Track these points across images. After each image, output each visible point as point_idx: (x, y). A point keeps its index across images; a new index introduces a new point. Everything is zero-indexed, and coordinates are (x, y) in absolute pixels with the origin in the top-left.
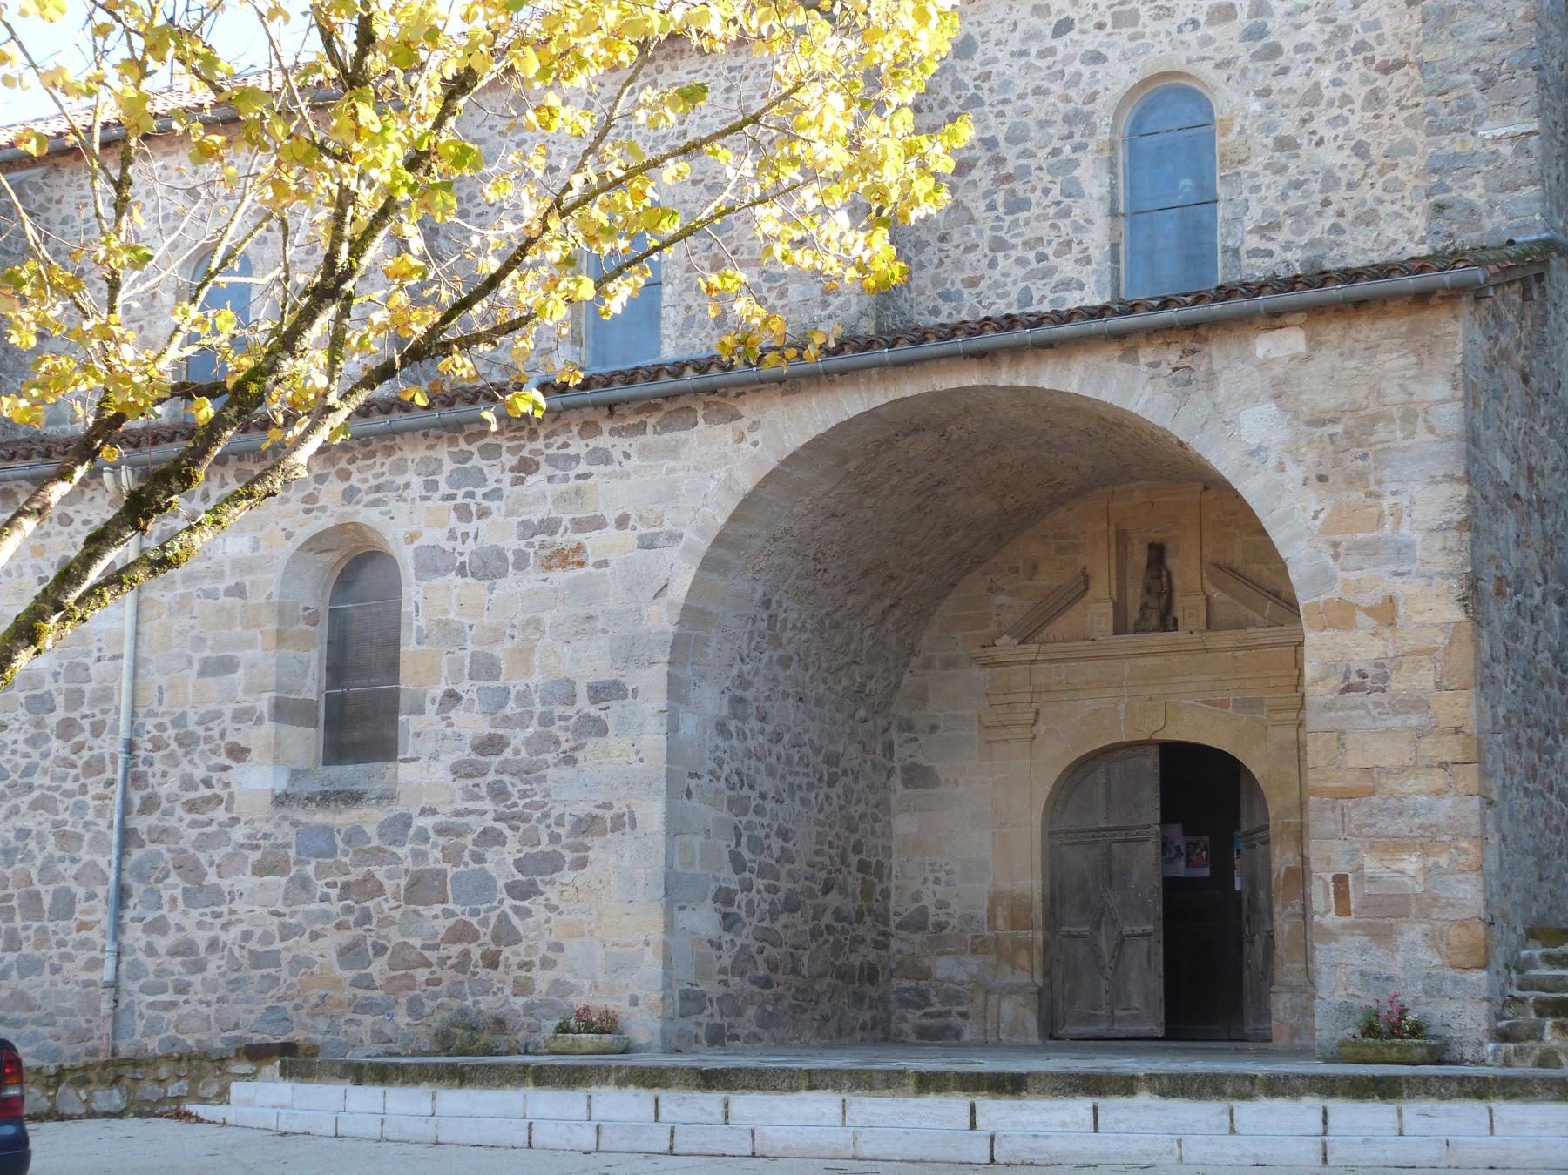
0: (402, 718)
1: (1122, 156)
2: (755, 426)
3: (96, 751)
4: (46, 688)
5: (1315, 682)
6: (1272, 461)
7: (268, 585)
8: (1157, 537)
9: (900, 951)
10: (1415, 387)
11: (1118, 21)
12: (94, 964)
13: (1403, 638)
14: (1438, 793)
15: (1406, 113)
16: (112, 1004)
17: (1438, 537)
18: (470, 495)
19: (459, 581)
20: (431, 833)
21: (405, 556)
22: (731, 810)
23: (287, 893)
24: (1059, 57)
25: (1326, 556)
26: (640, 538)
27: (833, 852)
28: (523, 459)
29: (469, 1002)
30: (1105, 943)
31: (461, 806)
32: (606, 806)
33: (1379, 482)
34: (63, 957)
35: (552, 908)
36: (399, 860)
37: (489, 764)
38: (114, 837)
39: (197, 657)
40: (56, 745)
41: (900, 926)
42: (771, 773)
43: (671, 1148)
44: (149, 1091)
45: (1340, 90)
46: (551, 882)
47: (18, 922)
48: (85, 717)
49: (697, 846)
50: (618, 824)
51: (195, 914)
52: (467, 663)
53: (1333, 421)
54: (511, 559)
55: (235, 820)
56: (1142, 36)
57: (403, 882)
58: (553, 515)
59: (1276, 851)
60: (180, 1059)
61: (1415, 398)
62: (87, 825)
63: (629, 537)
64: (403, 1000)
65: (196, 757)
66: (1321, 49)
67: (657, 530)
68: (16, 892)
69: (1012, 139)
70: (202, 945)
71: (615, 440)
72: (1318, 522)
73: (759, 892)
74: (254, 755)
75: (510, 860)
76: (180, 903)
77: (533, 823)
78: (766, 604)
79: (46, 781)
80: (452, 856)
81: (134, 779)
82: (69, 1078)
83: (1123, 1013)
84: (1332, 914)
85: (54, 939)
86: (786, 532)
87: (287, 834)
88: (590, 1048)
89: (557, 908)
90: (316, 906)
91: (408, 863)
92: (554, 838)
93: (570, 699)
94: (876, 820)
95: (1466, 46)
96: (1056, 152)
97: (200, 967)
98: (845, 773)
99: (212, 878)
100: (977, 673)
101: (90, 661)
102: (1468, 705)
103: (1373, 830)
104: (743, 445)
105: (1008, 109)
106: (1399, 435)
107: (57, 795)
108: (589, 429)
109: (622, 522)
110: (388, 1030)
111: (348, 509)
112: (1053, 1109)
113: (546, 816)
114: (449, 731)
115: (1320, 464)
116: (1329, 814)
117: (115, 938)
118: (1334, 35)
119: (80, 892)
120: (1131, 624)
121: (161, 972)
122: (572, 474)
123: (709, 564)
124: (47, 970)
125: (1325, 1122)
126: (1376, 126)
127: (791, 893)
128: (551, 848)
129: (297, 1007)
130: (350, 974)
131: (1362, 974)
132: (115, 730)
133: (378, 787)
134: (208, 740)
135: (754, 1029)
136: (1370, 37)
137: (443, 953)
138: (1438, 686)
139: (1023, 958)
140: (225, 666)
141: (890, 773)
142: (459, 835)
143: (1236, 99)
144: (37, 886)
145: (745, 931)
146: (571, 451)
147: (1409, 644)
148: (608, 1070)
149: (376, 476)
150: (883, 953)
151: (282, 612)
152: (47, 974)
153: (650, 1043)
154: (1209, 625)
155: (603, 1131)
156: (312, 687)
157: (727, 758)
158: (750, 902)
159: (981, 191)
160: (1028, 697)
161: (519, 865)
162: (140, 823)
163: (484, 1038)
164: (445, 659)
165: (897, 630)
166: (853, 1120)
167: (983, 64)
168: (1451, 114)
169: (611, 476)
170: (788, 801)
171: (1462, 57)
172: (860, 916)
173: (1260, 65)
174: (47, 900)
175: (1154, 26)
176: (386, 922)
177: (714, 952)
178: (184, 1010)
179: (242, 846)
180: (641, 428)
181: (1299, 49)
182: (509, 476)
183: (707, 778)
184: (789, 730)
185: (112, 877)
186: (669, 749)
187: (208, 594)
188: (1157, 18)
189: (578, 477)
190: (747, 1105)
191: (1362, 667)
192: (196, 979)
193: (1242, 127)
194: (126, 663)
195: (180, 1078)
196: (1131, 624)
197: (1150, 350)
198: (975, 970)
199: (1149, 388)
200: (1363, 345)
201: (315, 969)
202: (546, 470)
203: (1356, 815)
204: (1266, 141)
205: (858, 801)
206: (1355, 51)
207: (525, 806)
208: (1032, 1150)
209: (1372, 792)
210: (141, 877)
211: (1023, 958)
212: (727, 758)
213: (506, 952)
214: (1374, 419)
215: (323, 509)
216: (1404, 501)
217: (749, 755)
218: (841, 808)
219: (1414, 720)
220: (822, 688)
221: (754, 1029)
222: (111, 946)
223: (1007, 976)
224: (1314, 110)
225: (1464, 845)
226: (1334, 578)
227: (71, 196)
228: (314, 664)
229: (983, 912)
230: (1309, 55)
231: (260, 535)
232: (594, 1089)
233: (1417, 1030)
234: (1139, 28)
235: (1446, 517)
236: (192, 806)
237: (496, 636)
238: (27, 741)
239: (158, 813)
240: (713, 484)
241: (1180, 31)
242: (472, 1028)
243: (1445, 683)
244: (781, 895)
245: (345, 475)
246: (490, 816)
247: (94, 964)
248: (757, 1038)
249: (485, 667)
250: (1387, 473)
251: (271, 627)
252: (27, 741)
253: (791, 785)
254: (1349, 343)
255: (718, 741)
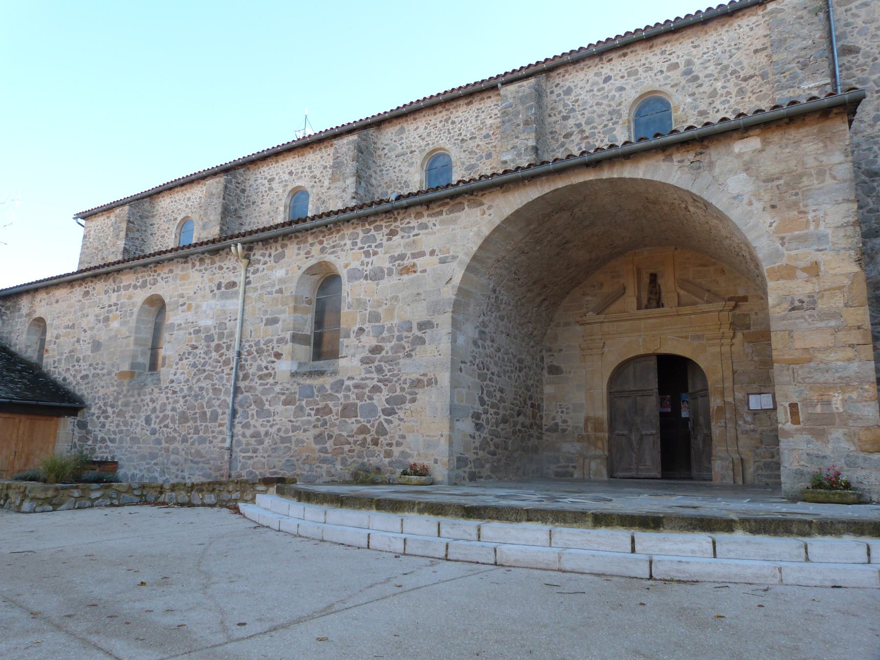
0: (341, 340)
1: (632, 126)
2: (490, 207)
3: (228, 356)
4: (211, 332)
5: (774, 306)
6: (746, 200)
7: (291, 288)
8: (653, 271)
9: (547, 440)
10: (824, 159)
11: (629, 74)
12: (224, 441)
13: (823, 282)
14: (849, 360)
15: (756, 95)
16: (229, 456)
17: (842, 230)
18: (370, 246)
19: (365, 282)
20: (352, 387)
21: (343, 273)
22: (479, 378)
23: (295, 412)
24: (606, 90)
25: (778, 244)
26: (440, 259)
27: (521, 399)
28: (391, 230)
29: (366, 460)
30: (634, 437)
31: (363, 376)
32: (425, 375)
33: (806, 206)
34: (213, 437)
35: (401, 420)
36: (338, 399)
37: (376, 358)
38: (232, 390)
39: (264, 318)
40: (214, 355)
41: (547, 430)
42: (496, 364)
43: (446, 555)
44: (225, 496)
45: (725, 90)
46: (401, 408)
47: (199, 423)
48: (224, 343)
49: (464, 393)
50: (430, 383)
51: (261, 420)
52: (367, 316)
53: (778, 179)
54: (386, 272)
55: (276, 383)
56: (640, 79)
57: (340, 408)
58: (403, 252)
59: (712, 399)
60: (237, 483)
61: (824, 163)
62: (223, 385)
63: (435, 259)
64: (339, 459)
65: (263, 358)
66: (716, 75)
67: (447, 255)
68: (198, 411)
69: (587, 123)
70: (263, 433)
71: (430, 219)
72: (773, 228)
73: (491, 414)
74: (284, 356)
75: (384, 399)
76: (255, 416)
77: (393, 383)
78: (494, 291)
79: (210, 368)
80: (360, 397)
81: (240, 367)
82: (196, 488)
83: (642, 467)
84: (789, 423)
85: (210, 430)
86: (504, 258)
87: (295, 388)
88: (416, 482)
89: (403, 419)
90: (306, 418)
91: (342, 400)
92: (402, 389)
93: (410, 329)
94: (538, 387)
95: (793, 52)
96: (606, 126)
97: (261, 442)
98: (525, 367)
99: (267, 406)
100: (578, 328)
101: (227, 321)
102: (865, 314)
103: (812, 380)
104: (485, 216)
105: (586, 112)
106: (815, 182)
107: (213, 373)
108: (419, 215)
109: (432, 253)
110: (333, 471)
111: (322, 256)
112: (685, 542)
113: (399, 379)
114: (360, 345)
115: (772, 200)
116: (785, 372)
117: (231, 430)
118: (722, 69)
119: (220, 411)
120: (643, 306)
121: (248, 444)
122: (411, 235)
123: (470, 269)
124: (208, 442)
125: (869, 555)
126: (742, 102)
127: (504, 415)
128: (401, 394)
129: (298, 460)
130: (318, 447)
131: (808, 454)
132: (234, 348)
133: (331, 369)
134: (268, 351)
135: (489, 473)
136: (738, 68)
137: (356, 439)
138: (846, 305)
139: (600, 444)
140: (274, 321)
141: (542, 369)
142: (363, 388)
143: (680, 98)
144: (206, 409)
145: (485, 432)
146: (411, 225)
147: (827, 285)
148: (414, 504)
149: (333, 242)
150: (540, 441)
151: (296, 299)
152: (208, 444)
153: (443, 481)
154: (679, 305)
155: (408, 542)
156: (308, 329)
157: (477, 356)
158: (487, 419)
159: (575, 143)
160: (600, 337)
161: (388, 401)
162: (242, 384)
163: (372, 476)
164: (358, 315)
165: (546, 310)
166: (556, 543)
167: (575, 97)
168: (787, 81)
169: (428, 234)
170: (503, 377)
171: (791, 57)
172: (531, 425)
173: (690, 84)
174: (208, 414)
175: (644, 75)
176: (333, 425)
177: (472, 440)
178: (256, 460)
179: (278, 393)
180: (441, 213)
181: (706, 76)
182: (386, 237)
183: (469, 364)
184: (503, 347)
185: (231, 406)
186: (452, 349)
187: (270, 293)
188: (646, 71)
189: (414, 236)
190: (492, 529)
191: (801, 297)
192: (260, 447)
193: (684, 108)
194: (239, 321)
195: (237, 491)
196: (643, 306)
197: (679, 155)
198: (579, 449)
199: (679, 172)
200: (792, 141)
201: (305, 444)
202: (401, 233)
203: (801, 372)
204: (694, 113)
205: (531, 379)
206: (731, 74)
207: (390, 375)
208: (678, 571)
209: (810, 361)
210: (242, 406)
211: (600, 444)
212: (477, 356)
213: (382, 439)
214: (801, 176)
215: (312, 256)
216: (820, 214)
217: (487, 356)
218: (524, 381)
219: (833, 323)
220: (517, 331)
221: (489, 473)
222: (229, 433)
223: (593, 452)
224: (714, 99)
225: (867, 387)
226: (783, 255)
227: (253, 178)
228: (309, 320)
229: (582, 425)
230: (711, 78)
231: (289, 268)
232: (406, 514)
233: (847, 486)
234: (639, 76)
235: (846, 220)
236: (261, 378)
237: (379, 304)
238: (204, 353)
239: (248, 381)
240: (472, 234)
241: (656, 75)
242: (367, 471)
243: (850, 303)
244: (500, 416)
245: (321, 242)
246: (376, 380)
247: (224, 441)
248: (490, 477)
249: (375, 317)
250: (810, 201)
251: (292, 305)
252: (204, 353)
253: (504, 370)
254: (785, 141)
255: (474, 348)
